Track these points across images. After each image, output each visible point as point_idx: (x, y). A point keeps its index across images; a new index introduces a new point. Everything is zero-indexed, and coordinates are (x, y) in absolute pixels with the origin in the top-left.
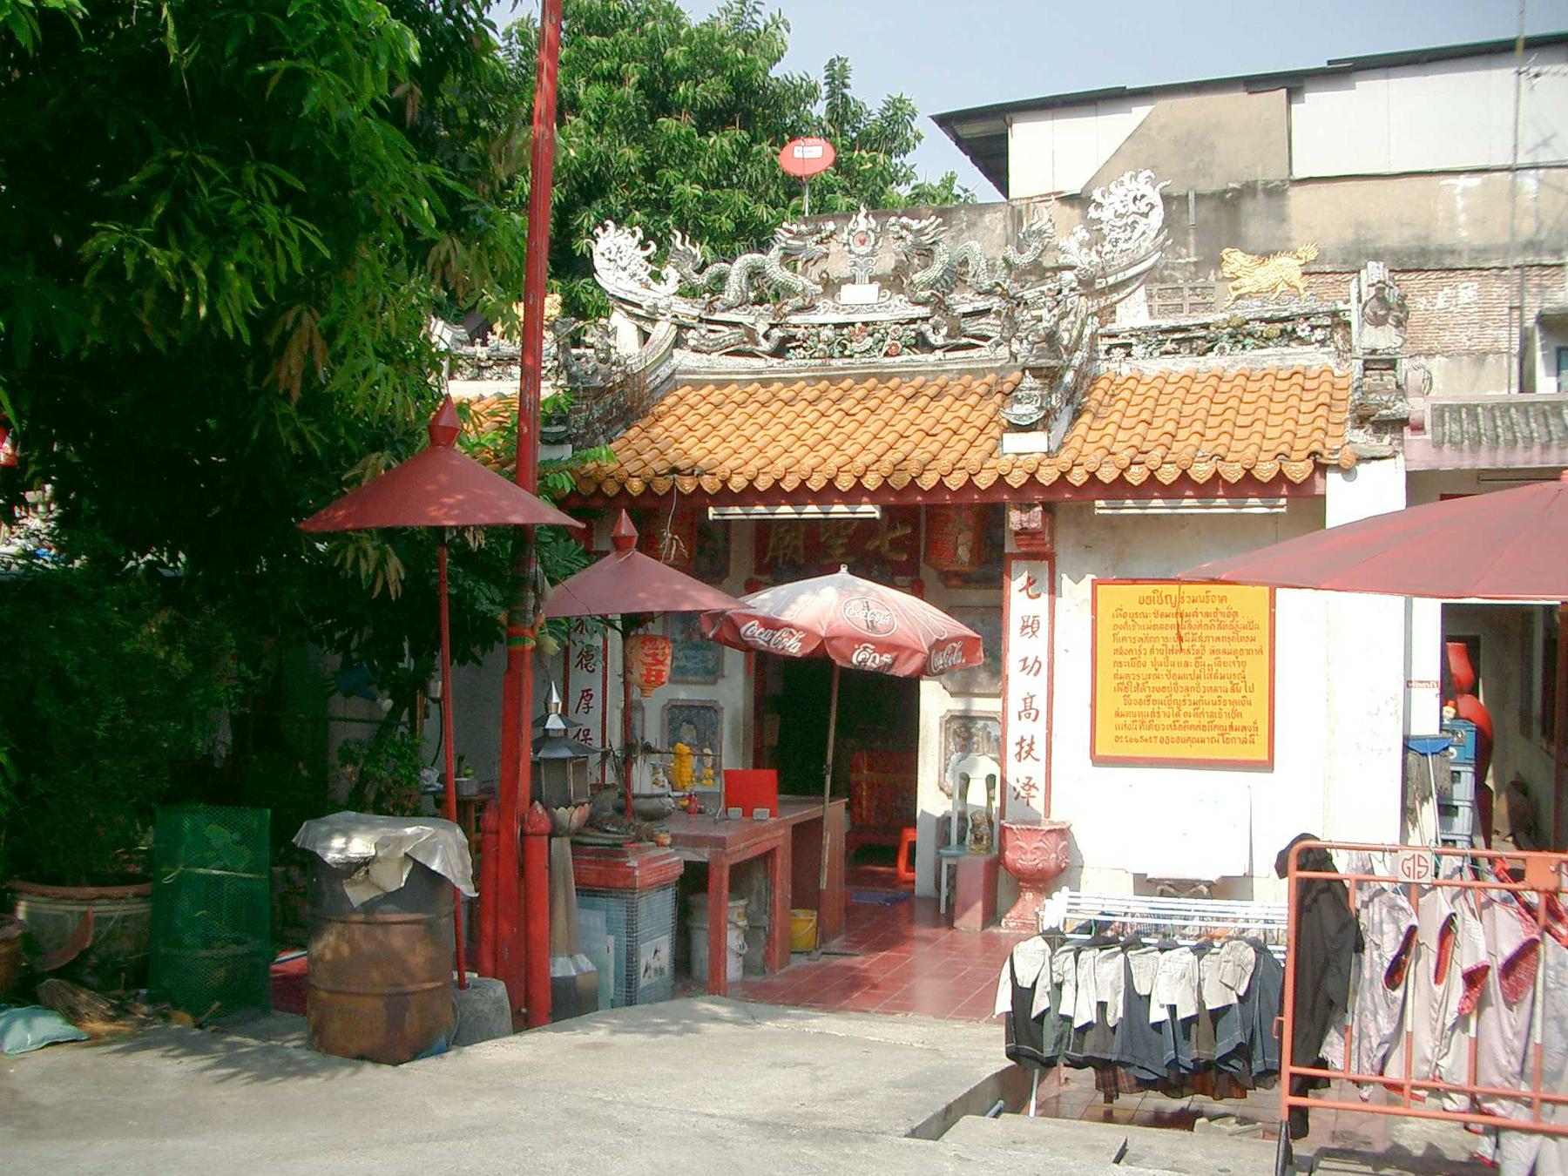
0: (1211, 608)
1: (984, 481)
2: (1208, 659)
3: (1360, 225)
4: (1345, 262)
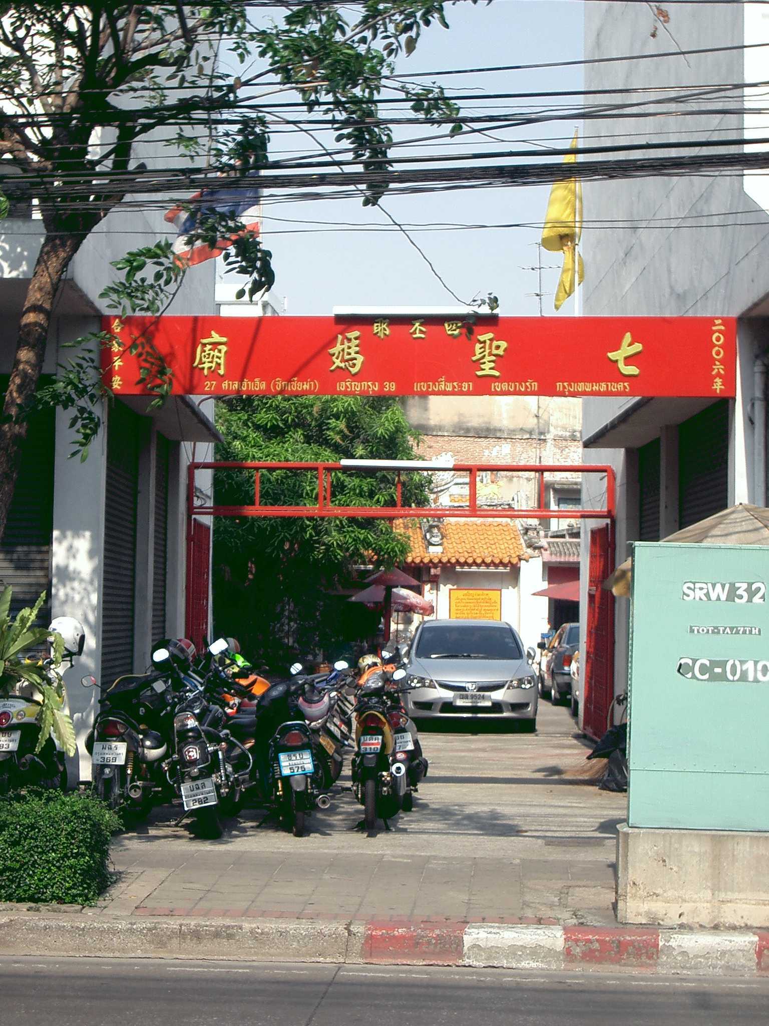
0: (483, 597)
1: (426, 560)
2: (483, 612)
3: (460, 415)
4: (453, 431)
